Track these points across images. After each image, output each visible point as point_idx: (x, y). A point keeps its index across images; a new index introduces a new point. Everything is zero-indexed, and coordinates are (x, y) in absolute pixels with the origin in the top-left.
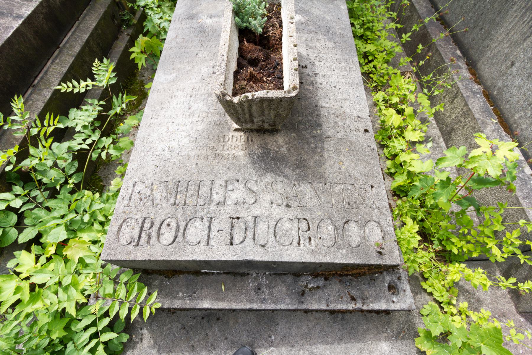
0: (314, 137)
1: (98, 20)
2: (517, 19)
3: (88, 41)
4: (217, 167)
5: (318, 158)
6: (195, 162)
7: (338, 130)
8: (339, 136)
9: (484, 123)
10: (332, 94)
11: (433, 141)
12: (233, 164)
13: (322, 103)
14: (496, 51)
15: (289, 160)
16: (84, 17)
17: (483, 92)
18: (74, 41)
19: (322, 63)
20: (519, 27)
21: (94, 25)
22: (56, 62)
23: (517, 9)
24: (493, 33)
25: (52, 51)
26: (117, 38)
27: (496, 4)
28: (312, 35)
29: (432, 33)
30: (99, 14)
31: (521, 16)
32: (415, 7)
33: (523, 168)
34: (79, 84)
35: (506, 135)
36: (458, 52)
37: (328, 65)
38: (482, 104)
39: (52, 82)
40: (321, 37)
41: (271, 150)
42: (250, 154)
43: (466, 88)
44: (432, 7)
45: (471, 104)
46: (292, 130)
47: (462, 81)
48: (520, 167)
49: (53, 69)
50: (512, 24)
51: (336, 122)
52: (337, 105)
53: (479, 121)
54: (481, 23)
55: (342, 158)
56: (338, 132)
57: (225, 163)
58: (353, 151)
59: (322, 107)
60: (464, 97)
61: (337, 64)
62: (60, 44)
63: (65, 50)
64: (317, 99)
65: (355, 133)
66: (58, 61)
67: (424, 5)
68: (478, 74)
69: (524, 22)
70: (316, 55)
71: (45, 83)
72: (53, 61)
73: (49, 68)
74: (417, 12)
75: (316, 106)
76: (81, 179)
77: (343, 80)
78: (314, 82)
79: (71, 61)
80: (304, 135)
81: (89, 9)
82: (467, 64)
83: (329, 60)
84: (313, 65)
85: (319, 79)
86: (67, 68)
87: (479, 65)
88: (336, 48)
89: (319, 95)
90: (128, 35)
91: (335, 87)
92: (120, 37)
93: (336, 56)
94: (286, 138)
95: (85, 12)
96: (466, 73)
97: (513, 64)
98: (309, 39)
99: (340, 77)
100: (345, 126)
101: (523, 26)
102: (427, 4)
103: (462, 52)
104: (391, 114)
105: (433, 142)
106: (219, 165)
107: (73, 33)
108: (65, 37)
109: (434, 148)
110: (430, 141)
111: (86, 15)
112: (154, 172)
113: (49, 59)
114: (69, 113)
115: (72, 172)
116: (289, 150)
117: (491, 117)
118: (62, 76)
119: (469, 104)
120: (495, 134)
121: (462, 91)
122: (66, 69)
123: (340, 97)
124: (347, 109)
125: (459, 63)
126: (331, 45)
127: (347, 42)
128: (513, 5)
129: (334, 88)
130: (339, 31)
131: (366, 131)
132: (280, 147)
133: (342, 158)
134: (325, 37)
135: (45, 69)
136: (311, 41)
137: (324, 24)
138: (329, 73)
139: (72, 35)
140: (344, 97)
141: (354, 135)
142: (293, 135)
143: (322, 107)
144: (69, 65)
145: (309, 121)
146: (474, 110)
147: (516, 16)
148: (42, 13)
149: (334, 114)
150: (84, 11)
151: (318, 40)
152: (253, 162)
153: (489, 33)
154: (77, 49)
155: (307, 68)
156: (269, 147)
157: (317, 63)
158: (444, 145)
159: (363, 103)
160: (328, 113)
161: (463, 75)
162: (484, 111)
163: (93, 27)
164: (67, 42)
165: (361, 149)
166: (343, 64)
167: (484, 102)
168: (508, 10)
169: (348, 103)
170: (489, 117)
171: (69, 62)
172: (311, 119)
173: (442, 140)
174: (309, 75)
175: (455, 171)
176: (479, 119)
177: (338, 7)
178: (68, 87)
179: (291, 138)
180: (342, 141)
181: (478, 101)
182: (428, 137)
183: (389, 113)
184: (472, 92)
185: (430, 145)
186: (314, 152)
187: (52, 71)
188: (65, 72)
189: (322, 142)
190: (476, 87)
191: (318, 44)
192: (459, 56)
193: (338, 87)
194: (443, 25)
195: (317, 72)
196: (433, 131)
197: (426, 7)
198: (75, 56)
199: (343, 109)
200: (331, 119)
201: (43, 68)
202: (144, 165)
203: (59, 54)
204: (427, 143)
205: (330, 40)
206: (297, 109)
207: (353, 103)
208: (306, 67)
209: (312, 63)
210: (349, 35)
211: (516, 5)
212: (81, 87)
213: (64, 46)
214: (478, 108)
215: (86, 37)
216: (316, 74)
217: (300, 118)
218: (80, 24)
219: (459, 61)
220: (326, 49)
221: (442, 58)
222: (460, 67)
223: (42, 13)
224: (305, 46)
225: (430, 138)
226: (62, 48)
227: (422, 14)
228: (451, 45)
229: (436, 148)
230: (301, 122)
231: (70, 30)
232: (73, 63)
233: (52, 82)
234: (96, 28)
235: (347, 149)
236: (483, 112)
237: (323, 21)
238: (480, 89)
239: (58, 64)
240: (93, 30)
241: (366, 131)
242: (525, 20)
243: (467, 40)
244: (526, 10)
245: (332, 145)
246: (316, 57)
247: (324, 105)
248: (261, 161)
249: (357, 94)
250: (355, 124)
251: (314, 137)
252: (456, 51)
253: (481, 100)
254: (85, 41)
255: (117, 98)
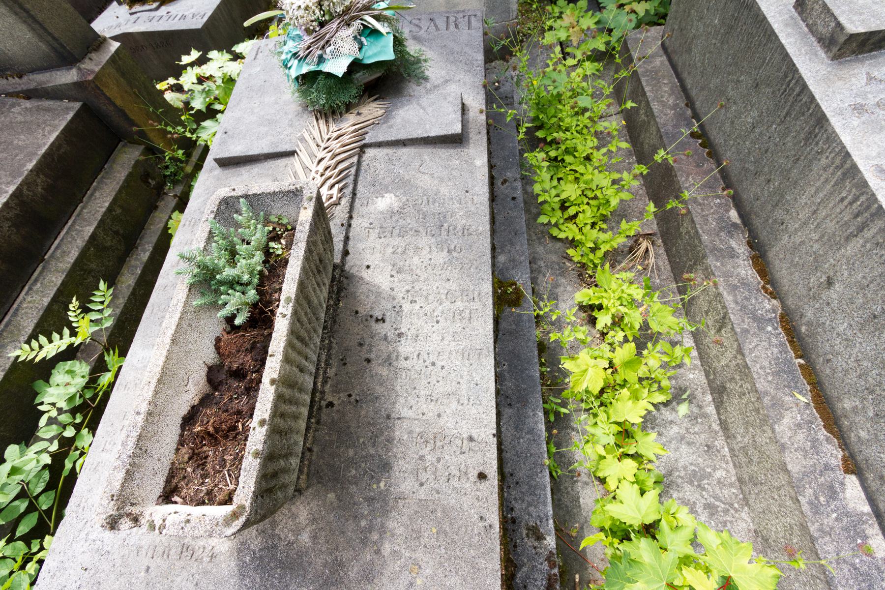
0: (371, 500)
1: (114, 193)
2: (828, 187)
3: (93, 237)
4: (179, 579)
5: (369, 557)
6: (146, 562)
7: (423, 477)
8: (422, 493)
9: (777, 404)
10: (424, 382)
11: (691, 399)
12: (206, 573)
13: (402, 409)
14: (798, 240)
15: (310, 564)
16: (92, 195)
17: (782, 317)
18: (70, 242)
19: (417, 306)
20: (835, 206)
21: (107, 204)
22: (35, 288)
23: (828, 166)
24: (788, 198)
25: (31, 271)
26: (156, 208)
27: (789, 139)
28: (408, 238)
29: (680, 169)
30: (118, 183)
31: (836, 184)
32: (651, 108)
33: (866, 537)
34: (50, 341)
35: (827, 439)
36: (733, 214)
37: (428, 308)
38: (776, 350)
39: (24, 327)
40: (425, 241)
41: (280, 539)
42: (239, 551)
43: (743, 308)
44: (687, 105)
45: (751, 351)
46: (329, 485)
47: (733, 288)
48: (858, 534)
49: (29, 302)
50: (821, 195)
51: (422, 458)
52: (431, 410)
53: (766, 401)
54: (766, 169)
55: (419, 555)
56: (422, 485)
57: (194, 571)
58: (446, 533)
59: (399, 419)
60: (736, 333)
61: (447, 304)
62: (45, 254)
63: (53, 263)
64: (393, 398)
65: (457, 485)
66: (39, 285)
67: (671, 102)
68: (772, 274)
69: (842, 200)
70: (407, 288)
71: (12, 332)
72: (30, 289)
73: (21, 303)
74: (655, 120)
75: (388, 417)
76: (52, 502)
77: (453, 344)
78: (393, 356)
79: (60, 282)
80: (352, 497)
81: (103, 177)
82: (751, 245)
83: (431, 298)
84: (398, 310)
85: (405, 348)
86: (52, 296)
87: (771, 254)
88: (451, 263)
89: (398, 388)
90: (175, 196)
91: (433, 364)
92: (161, 204)
93: (448, 285)
94: (314, 505)
95: (95, 184)
96: (746, 270)
97: (830, 283)
98: (399, 250)
99: (448, 337)
100: (439, 466)
101: (842, 206)
102: (677, 98)
103: (741, 216)
104: (584, 367)
105: (690, 402)
106: (184, 574)
107: (69, 228)
108: (55, 239)
109: (693, 418)
110: (685, 400)
111: (95, 190)
112: (78, 583)
113: (24, 286)
114: (51, 374)
115: (39, 490)
116: (314, 537)
117: (796, 387)
118: (41, 313)
119: (746, 352)
120: (801, 436)
121: (732, 316)
122: (50, 299)
123: (441, 388)
124: (448, 423)
125: (733, 243)
126: (440, 257)
127: (475, 247)
128: (818, 153)
129: (431, 368)
130: (464, 222)
131: (482, 476)
132: (297, 532)
133: (419, 555)
134: (433, 240)
135: (15, 306)
136: (404, 252)
137: (434, 208)
138: (427, 328)
139: (67, 233)
140: (449, 389)
141: (454, 489)
142: (331, 496)
143: (399, 419)
144: (55, 289)
145: (366, 458)
146: (755, 369)
147: (827, 181)
148: (7, 219)
149: (421, 435)
150: (92, 184)
151: (418, 249)
152: (243, 568)
153: (782, 196)
154: (74, 254)
155: (384, 322)
156: (277, 531)
157: (406, 307)
158: (714, 412)
159: (484, 402)
160: (410, 433)
161: (738, 274)
162: (781, 370)
163: (104, 210)
164: (57, 248)
165: (464, 529)
166: (459, 304)
167: (781, 344)
168: (811, 161)
169: (454, 405)
170: (789, 387)
171: (55, 285)
172: (372, 451)
173: (709, 398)
174: (386, 338)
175: (733, 479)
176: (767, 393)
177: (470, 162)
178: (32, 350)
179: (324, 506)
180: (426, 509)
181: (766, 344)
182: (681, 389)
183: (579, 366)
184: (755, 318)
185: (683, 409)
186: (364, 542)
187: (26, 308)
188: (46, 304)
189: (385, 513)
190: (768, 305)
191: (416, 260)
192: (734, 225)
193: (439, 364)
194: (705, 147)
195: (403, 330)
196: (691, 376)
197: (675, 107)
198: (68, 269)
199: (442, 422)
200: (412, 453)
201: (13, 304)
202: (67, 565)
203: (41, 273)
204: (678, 404)
205: (440, 246)
206: (349, 427)
207: (466, 402)
208: (383, 320)
209: (397, 309)
210: (481, 229)
211: (824, 156)
212: (50, 348)
213: (52, 256)
214: (766, 364)
215: (90, 230)
216: (400, 335)
217: (351, 452)
218: (83, 208)
219: (732, 237)
220: (430, 268)
221: (697, 232)
222: (733, 254)
223: (7, 219)
224: (390, 267)
225: (685, 391)
226: (48, 262)
227: (665, 125)
228: (718, 197)
229: (696, 418)
230: (351, 462)
231: (66, 223)
232: (62, 284)
233: (24, 327)
234: (110, 210)
235: (434, 530)
236: (777, 374)
237: (434, 202)
238: (774, 311)
239: (37, 292)
240: (105, 214)
241: (482, 476)
242: (844, 194)
243: (751, 191)
244: (844, 174)
245: (404, 519)
246: (408, 291)
247: (405, 412)
248: (255, 569)
249: (477, 379)
250: (462, 458)
251: (371, 500)
252: (728, 211)
253: (774, 340)
254: (87, 238)
255: (109, 354)
